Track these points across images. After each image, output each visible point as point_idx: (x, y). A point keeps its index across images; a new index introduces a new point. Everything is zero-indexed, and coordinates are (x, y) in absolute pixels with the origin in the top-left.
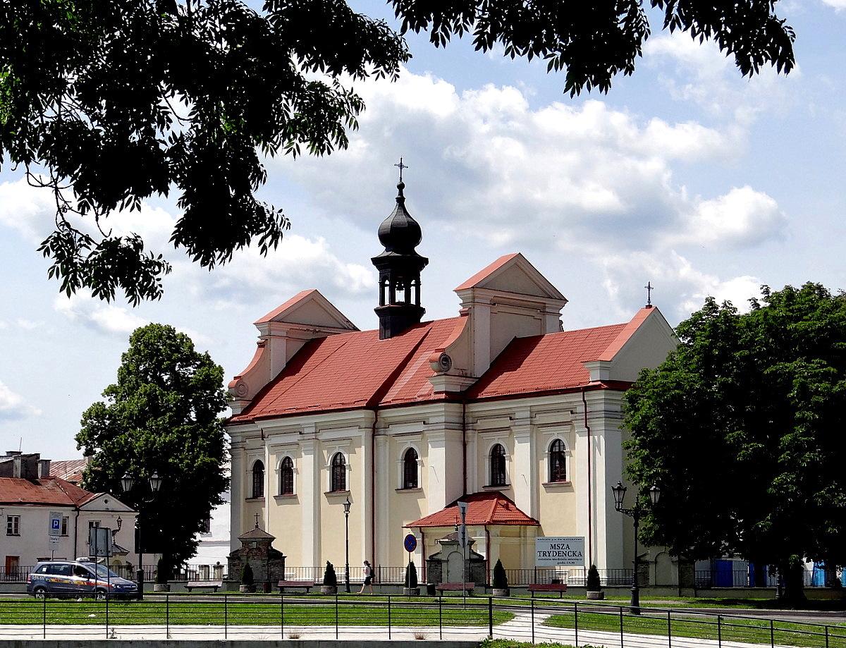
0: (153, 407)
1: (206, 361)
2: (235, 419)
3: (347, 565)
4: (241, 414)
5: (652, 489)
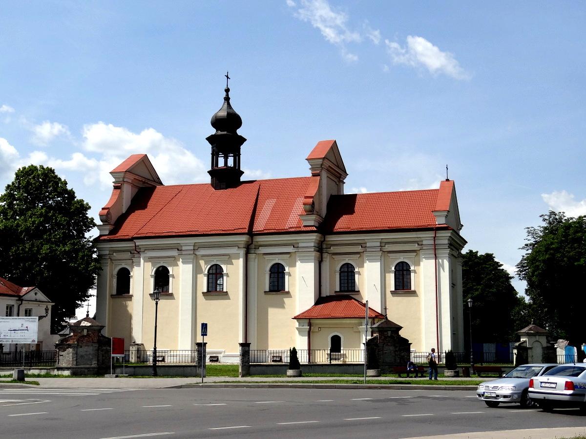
3: (155, 348)
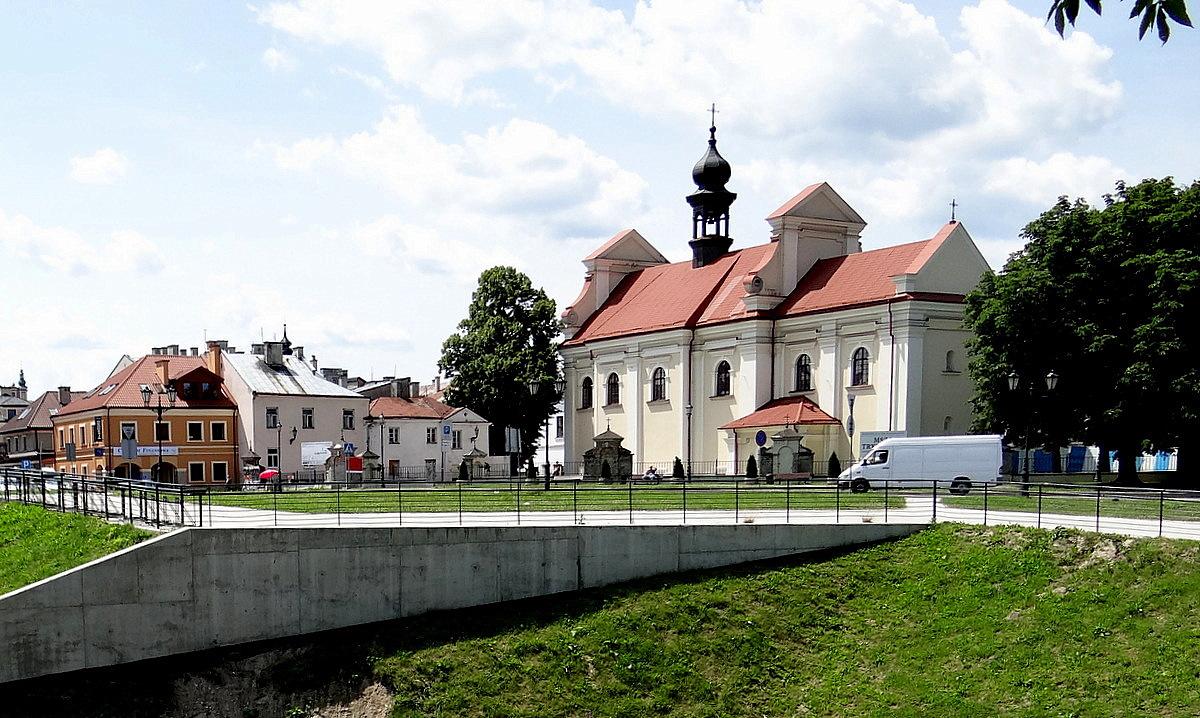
0: (499, 336)
1: (541, 296)
2: (567, 343)
4: (573, 339)
5: (1049, 375)
